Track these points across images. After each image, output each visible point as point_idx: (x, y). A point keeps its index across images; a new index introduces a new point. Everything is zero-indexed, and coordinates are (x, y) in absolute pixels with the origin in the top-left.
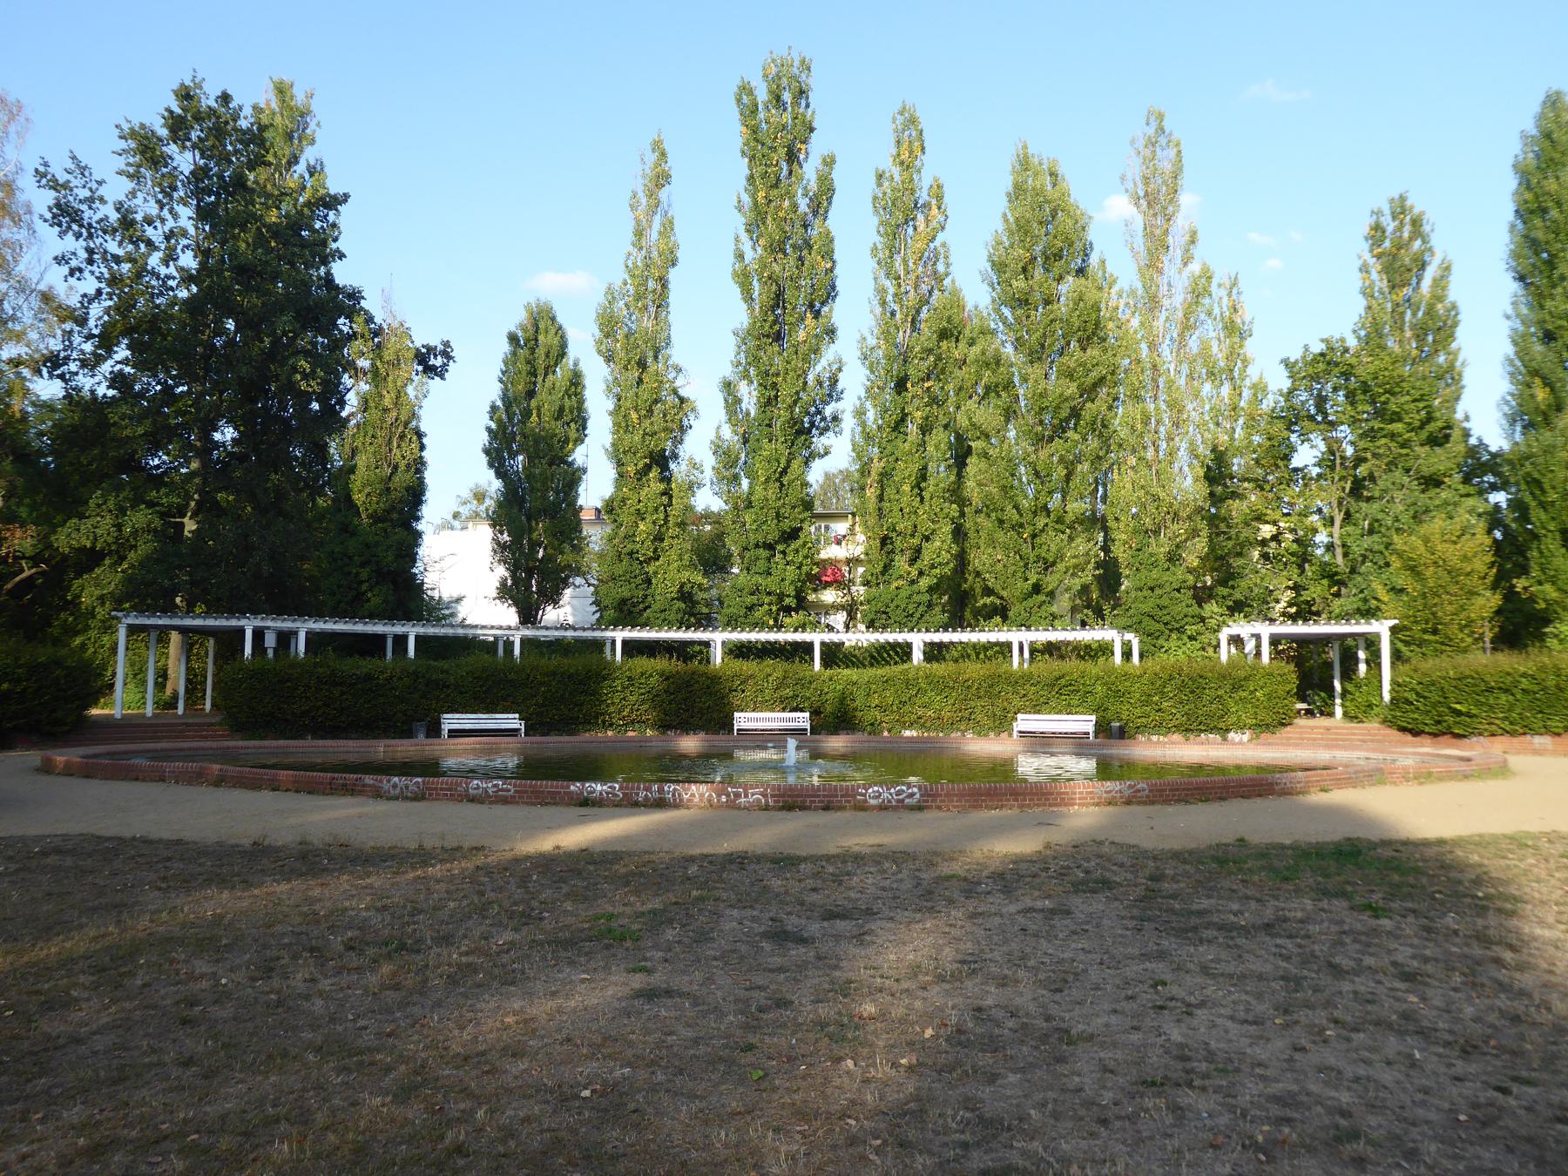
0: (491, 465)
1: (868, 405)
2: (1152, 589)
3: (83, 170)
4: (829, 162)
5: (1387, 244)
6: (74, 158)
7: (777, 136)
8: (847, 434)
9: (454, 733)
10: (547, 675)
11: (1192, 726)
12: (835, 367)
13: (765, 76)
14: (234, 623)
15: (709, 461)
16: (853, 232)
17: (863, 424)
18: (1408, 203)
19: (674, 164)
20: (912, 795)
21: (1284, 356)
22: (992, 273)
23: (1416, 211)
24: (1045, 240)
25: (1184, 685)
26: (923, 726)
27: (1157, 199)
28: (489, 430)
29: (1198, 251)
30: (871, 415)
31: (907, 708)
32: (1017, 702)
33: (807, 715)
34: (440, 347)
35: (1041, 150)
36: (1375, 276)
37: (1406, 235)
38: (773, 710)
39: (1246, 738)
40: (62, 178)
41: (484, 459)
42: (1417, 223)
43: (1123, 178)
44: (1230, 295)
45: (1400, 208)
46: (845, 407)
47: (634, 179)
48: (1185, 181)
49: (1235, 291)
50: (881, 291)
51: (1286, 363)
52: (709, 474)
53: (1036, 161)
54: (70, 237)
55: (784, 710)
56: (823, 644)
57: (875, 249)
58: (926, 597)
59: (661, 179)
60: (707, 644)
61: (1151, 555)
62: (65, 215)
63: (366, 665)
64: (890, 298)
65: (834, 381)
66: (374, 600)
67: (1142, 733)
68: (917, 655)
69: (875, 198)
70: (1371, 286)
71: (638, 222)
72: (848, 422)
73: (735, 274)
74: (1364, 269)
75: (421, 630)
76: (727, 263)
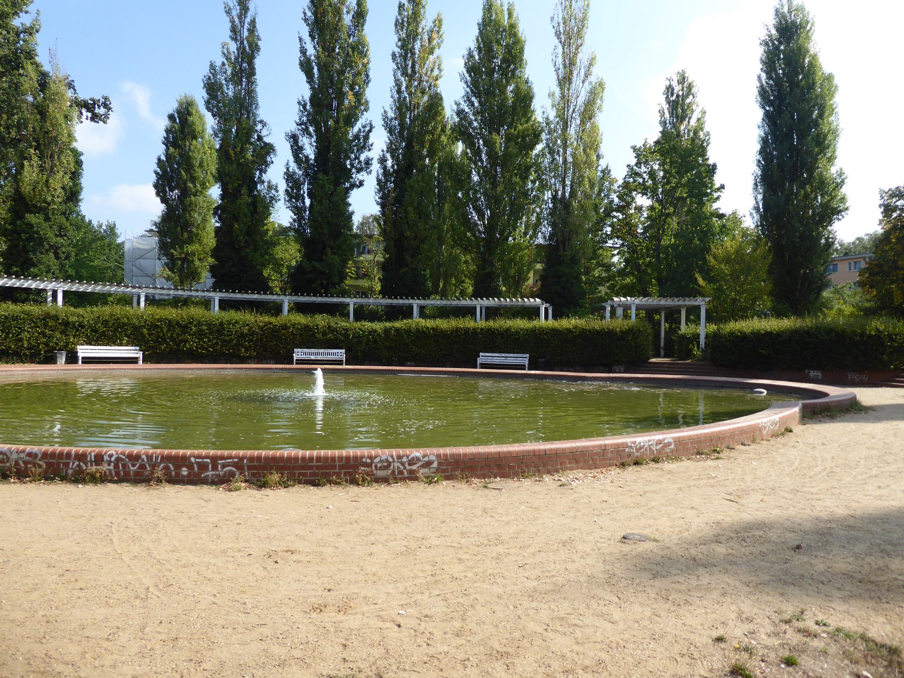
0: (158, 194)
1: (388, 155)
8: (374, 175)
12: (367, 129)
14: (406, 302)
15: (282, 186)
16: (380, 41)
17: (385, 168)
18: (686, 75)
21: (633, 144)
22: (467, 75)
23: (690, 80)
27: (570, 35)
29: (594, 70)
30: (389, 163)
33: (344, 351)
42: (690, 87)
43: (552, 19)
45: (682, 79)
50: (398, 84)
51: (634, 148)
52: (282, 194)
64: (403, 88)
65: (367, 137)
69: (397, 20)
71: (232, 22)
72: (376, 167)
73: (301, 64)
76: (296, 57)
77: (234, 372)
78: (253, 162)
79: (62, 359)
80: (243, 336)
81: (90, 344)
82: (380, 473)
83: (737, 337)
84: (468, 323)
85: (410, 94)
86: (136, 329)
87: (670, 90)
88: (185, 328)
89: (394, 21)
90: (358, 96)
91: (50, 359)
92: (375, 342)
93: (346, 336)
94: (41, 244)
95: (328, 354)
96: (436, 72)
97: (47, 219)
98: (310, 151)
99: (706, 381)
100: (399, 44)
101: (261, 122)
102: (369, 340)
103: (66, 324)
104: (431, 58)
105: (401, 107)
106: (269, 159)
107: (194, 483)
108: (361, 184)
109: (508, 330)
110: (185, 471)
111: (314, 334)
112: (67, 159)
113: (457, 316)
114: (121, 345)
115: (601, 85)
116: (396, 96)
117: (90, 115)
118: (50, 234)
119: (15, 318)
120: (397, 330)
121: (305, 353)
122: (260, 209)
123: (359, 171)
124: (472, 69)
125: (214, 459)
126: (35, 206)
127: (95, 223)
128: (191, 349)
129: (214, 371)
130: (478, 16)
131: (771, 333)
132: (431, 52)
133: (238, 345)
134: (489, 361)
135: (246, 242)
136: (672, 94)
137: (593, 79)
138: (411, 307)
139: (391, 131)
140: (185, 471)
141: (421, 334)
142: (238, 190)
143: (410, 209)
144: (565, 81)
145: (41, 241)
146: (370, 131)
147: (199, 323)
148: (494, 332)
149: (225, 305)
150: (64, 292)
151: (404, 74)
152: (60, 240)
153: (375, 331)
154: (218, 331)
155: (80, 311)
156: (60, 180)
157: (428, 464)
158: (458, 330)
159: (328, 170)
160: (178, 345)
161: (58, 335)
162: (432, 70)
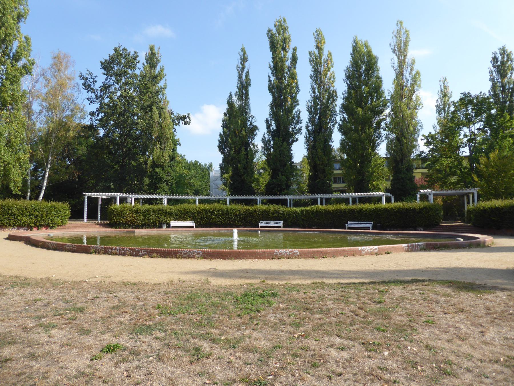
0: (220, 150)
1: (310, 125)
4: (295, 50)
5: (499, 63)
7: (278, 42)
9: (173, 227)
13: (275, 26)
17: (308, 131)
18: (506, 49)
19: (249, 54)
23: (509, 52)
24: (363, 66)
27: (400, 50)
28: (219, 141)
35: (362, 38)
36: (494, 74)
37: (505, 59)
40: (86, 76)
41: (218, 149)
44: (444, 84)
45: (503, 51)
46: (303, 125)
47: (236, 61)
48: (411, 44)
49: (445, 83)
50: (313, 89)
53: (360, 42)
54: (90, 93)
56: (102, 198)
59: (244, 59)
60: (162, 199)
62: (87, 87)
64: (316, 90)
68: (165, 202)
69: (310, 61)
70: (493, 79)
71: (239, 73)
72: (304, 131)
74: (491, 72)
75: (201, 197)
77: (226, 231)
78: (246, 135)
79: (165, 227)
80: (237, 215)
81: (175, 221)
82: (184, 255)
83: (482, 210)
84: (343, 207)
85: (320, 93)
86: (193, 214)
87: (495, 59)
88: (212, 213)
89: (309, 61)
90: (294, 98)
91: (161, 227)
92: (297, 217)
93: (283, 214)
94: (161, 180)
95: (275, 223)
96: (332, 79)
97: (163, 169)
98: (274, 127)
99: (443, 234)
100: (313, 70)
101: (252, 116)
102: (294, 216)
103: (166, 212)
104: (329, 73)
105: (315, 99)
106: (255, 133)
107: (136, 256)
108: (297, 140)
109: (361, 209)
110: (134, 253)
111: (268, 214)
112: (170, 144)
113: (278, 204)
114: (187, 221)
115: (418, 73)
116: (313, 95)
117: (183, 122)
118: (164, 176)
119: (148, 211)
120: (307, 211)
121: (265, 223)
122: (249, 157)
123: (296, 134)
124: (348, 77)
125: (141, 250)
126: (159, 165)
127: (203, 164)
128: (215, 222)
129: (217, 231)
130: (351, 50)
131: (499, 207)
132: (329, 71)
133: (235, 220)
134: (352, 225)
135: (244, 172)
136: (497, 62)
137: (414, 72)
138: (286, 200)
139: (310, 112)
140: (134, 253)
141: (319, 213)
142: (240, 149)
143: (319, 150)
144: (400, 75)
145: (160, 179)
146: (299, 114)
147: (218, 211)
148: (354, 211)
149: (232, 201)
150: (168, 199)
151: (316, 84)
152: (168, 178)
153: (297, 212)
154: (226, 214)
155: (172, 207)
156: (168, 152)
157: (199, 253)
158: (337, 210)
159: (282, 134)
160: (209, 220)
161: (163, 217)
162: (330, 79)
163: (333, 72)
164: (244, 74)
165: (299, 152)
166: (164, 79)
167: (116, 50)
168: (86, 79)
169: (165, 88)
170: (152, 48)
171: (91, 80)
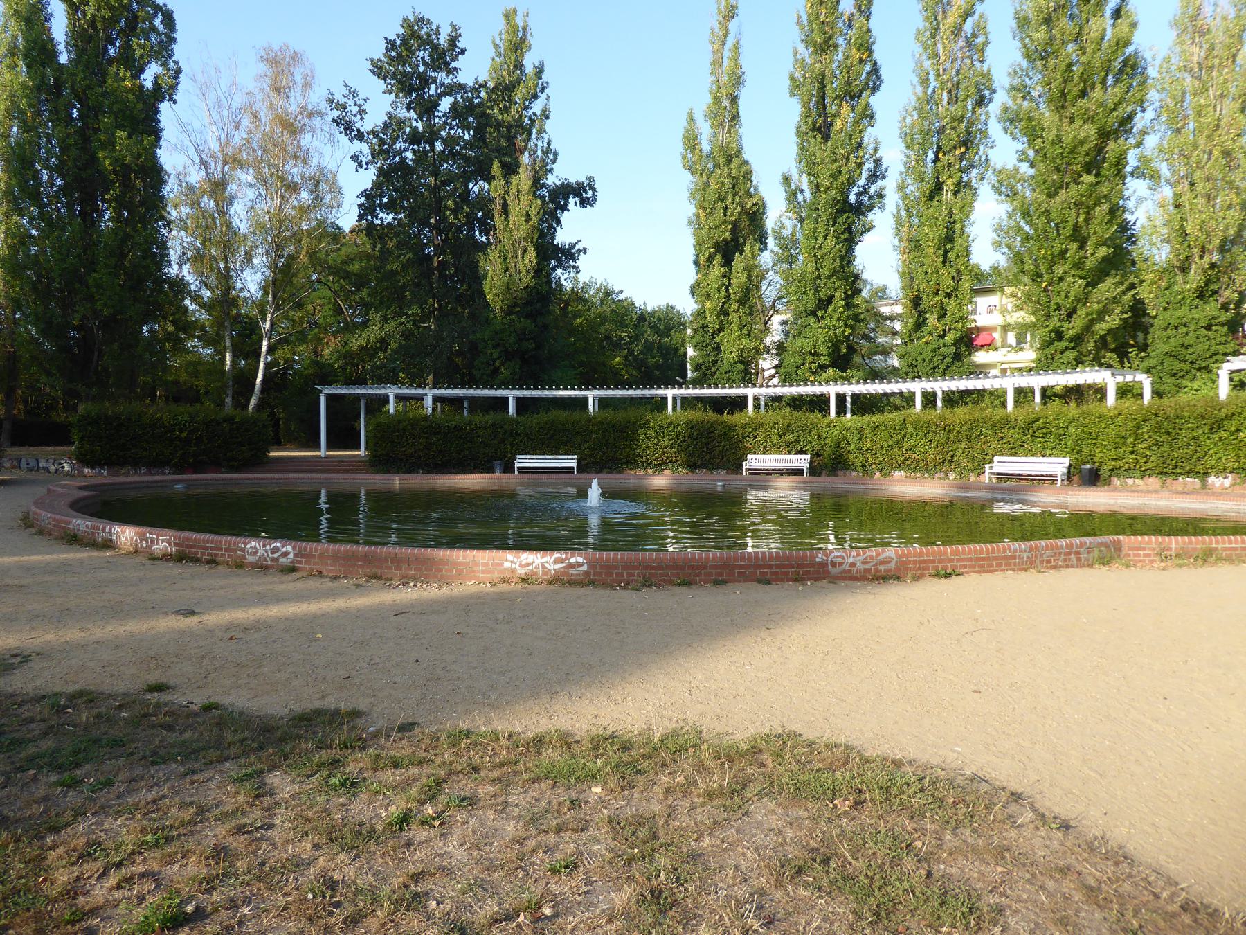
2: (1176, 328)
3: (354, 93)
6: (346, 86)
9: (522, 470)
10: (596, 425)
11: (1167, 470)
17: (905, 197)
20: (286, 554)
25: (1158, 426)
26: (909, 467)
31: (895, 451)
32: (995, 444)
34: (587, 182)
38: (780, 453)
39: (1227, 482)
40: (342, 100)
46: (889, 185)
55: (789, 453)
56: (854, 396)
57: (919, 33)
58: (953, 349)
61: (1178, 293)
63: (577, 415)
66: (505, 372)
67: (1117, 475)
68: (429, 401)
116: (919, 90)
117: (577, 200)
138: (665, 399)
163: (982, 16)
164: (727, 53)
165: (880, 259)
166: (544, 96)
167: (406, 24)
168: (344, 107)
169: (546, 115)
170: (509, 16)
171: (355, 109)
